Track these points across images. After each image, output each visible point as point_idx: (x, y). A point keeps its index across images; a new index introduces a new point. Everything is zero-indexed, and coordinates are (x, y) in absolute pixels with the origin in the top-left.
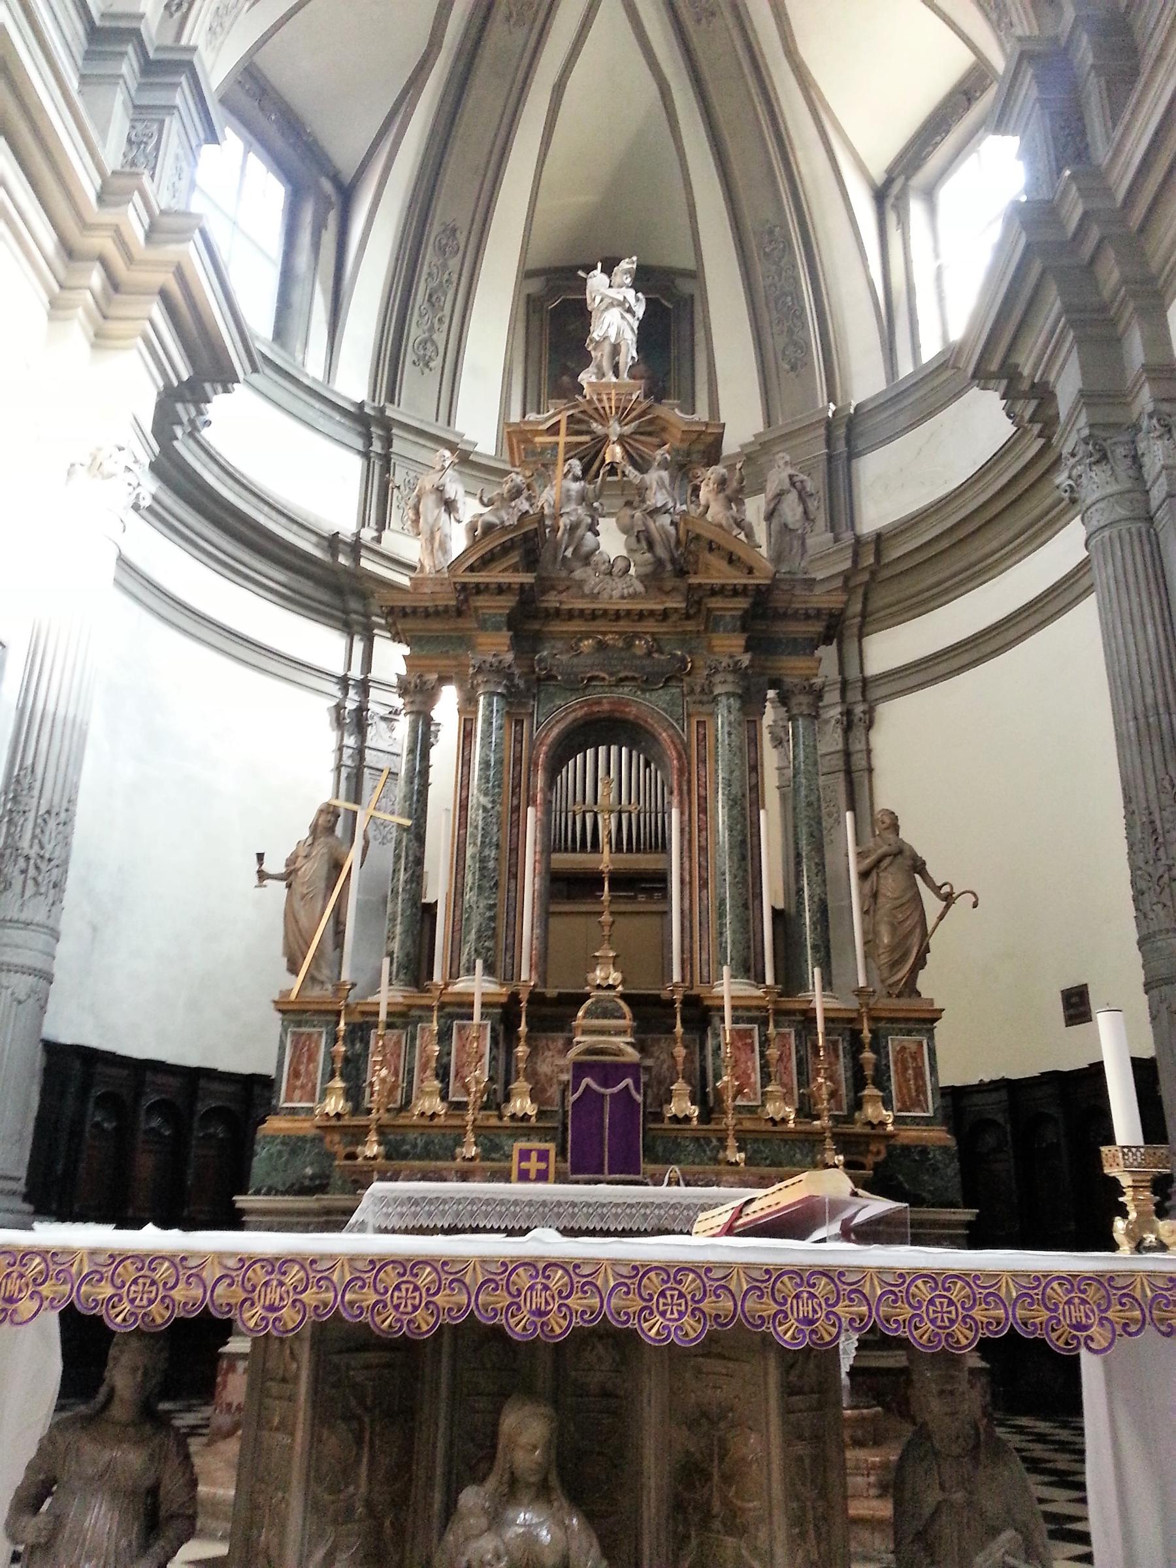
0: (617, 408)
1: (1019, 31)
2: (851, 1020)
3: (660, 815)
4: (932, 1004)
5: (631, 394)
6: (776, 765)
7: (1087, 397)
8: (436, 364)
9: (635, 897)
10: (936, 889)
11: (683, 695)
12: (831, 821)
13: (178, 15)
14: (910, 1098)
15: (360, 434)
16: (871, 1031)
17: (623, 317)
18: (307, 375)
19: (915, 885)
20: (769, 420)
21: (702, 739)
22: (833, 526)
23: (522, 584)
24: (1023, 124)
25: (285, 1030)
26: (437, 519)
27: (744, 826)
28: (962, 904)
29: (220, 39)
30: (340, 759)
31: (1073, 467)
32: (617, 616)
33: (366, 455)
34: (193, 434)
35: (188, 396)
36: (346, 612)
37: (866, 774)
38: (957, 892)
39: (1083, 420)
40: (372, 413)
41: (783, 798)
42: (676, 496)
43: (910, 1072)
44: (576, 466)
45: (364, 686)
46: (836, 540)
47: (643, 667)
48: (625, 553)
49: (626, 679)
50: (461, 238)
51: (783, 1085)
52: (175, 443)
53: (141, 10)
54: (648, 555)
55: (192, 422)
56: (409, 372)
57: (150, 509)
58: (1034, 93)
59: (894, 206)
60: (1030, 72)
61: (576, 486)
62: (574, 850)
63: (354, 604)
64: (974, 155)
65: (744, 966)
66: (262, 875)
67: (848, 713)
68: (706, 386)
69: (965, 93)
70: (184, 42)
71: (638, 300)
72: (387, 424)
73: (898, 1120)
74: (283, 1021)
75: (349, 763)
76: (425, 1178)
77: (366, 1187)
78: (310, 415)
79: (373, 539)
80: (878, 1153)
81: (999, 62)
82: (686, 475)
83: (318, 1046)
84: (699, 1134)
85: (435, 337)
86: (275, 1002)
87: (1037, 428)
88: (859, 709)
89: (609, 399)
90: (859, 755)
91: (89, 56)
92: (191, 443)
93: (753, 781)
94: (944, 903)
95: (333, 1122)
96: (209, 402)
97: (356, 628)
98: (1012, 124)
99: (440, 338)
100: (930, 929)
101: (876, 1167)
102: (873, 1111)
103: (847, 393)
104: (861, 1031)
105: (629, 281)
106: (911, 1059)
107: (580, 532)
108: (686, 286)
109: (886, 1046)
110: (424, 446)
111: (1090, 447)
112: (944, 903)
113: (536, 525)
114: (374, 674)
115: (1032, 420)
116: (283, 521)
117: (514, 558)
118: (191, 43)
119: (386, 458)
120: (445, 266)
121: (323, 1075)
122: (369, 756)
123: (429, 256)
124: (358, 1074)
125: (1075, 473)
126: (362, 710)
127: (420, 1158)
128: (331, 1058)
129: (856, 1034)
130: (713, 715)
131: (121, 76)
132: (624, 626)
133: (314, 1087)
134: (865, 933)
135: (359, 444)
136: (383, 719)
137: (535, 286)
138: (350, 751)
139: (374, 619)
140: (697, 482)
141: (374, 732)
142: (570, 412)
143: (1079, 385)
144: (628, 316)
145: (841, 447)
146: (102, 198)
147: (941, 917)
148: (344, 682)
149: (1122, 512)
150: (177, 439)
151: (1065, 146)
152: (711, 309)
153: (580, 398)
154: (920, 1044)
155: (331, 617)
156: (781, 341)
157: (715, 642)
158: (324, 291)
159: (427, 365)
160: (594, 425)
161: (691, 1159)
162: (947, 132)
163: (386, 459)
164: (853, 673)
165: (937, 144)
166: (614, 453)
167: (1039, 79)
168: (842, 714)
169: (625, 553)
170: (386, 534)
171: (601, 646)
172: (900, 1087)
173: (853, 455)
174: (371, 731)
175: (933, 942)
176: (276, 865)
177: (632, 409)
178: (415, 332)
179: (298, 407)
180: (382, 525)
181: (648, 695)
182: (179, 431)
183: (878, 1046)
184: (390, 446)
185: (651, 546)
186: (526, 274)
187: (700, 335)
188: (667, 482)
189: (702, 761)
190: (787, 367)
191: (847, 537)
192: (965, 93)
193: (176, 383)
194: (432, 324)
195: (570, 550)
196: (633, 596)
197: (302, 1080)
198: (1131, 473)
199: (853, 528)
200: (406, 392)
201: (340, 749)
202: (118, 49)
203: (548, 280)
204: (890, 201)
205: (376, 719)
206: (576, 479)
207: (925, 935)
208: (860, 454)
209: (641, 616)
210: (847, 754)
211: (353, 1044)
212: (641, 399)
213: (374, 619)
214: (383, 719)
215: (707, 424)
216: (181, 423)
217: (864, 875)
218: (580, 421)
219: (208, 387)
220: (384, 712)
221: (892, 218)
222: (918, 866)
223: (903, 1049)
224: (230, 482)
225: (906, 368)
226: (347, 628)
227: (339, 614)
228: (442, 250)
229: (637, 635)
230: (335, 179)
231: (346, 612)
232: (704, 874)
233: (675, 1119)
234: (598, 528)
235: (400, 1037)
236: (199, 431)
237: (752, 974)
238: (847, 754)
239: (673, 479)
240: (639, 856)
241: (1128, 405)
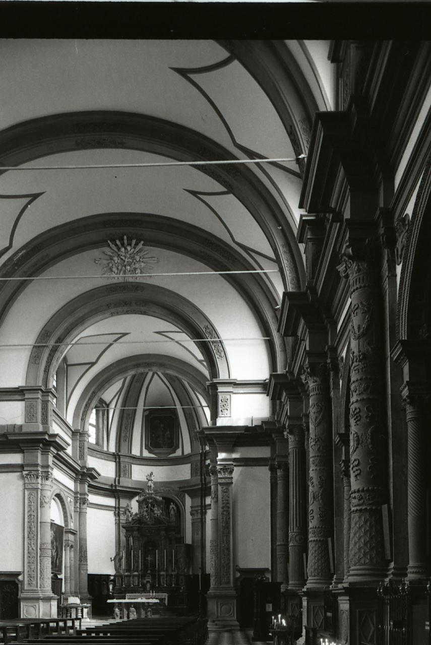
8: (127, 440)
20: (192, 451)
33: (115, 462)
36: (115, 495)
45: (119, 508)
50: (131, 416)
56: (122, 443)
63: (116, 494)
66: (111, 560)
72: (119, 456)
88: (204, 511)
91: (72, 435)
114: (121, 506)
122: (121, 521)
123: (125, 420)
126: (119, 513)
137: (147, 413)
145: (203, 458)
148: (115, 507)
163: (119, 462)
174: (121, 517)
176: (113, 559)
178: (123, 435)
201: (116, 520)
210: (202, 519)
226: (115, 497)
228: (127, 418)
230: (106, 404)
238: (202, 519)
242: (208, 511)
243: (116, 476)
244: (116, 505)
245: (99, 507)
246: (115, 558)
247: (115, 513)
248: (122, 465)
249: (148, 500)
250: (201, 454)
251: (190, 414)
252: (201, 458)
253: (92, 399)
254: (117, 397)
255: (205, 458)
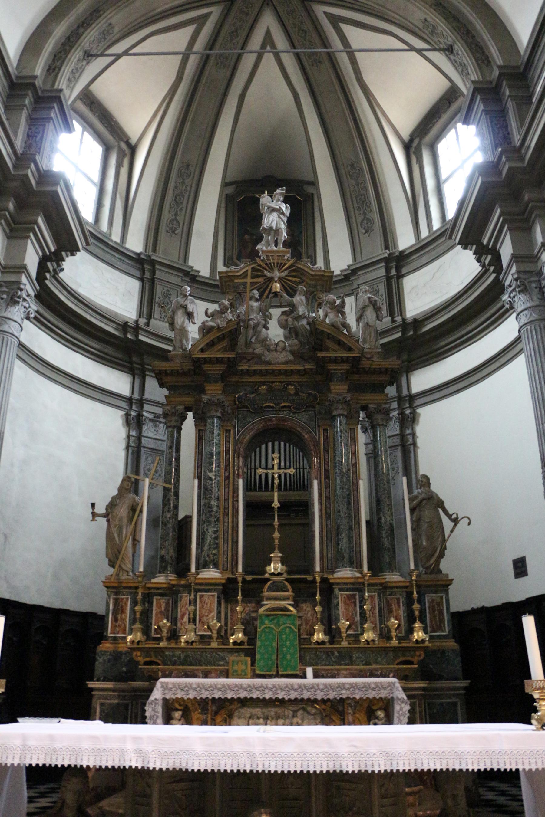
0: (278, 263)
1: (473, 78)
2: (406, 587)
3: (301, 470)
4: (448, 577)
5: (284, 256)
6: (364, 442)
7: (515, 258)
9: (289, 515)
10: (449, 516)
11: (316, 415)
12: (394, 472)
13: (53, 74)
14: (437, 625)
15: (138, 269)
16: (417, 593)
17: (279, 217)
18: (112, 241)
19: (439, 514)
21: (326, 439)
22: (391, 314)
23: (229, 358)
24: (477, 120)
25: (109, 596)
26: (183, 322)
27: (350, 486)
28: (463, 523)
29: (73, 83)
30: (128, 443)
31: (511, 292)
32: (280, 372)
33: (142, 280)
34: (55, 276)
35: (54, 258)
36: (131, 362)
37: (412, 447)
38: (460, 517)
39: (514, 269)
40: (145, 258)
41: (368, 460)
42: (309, 308)
43: (436, 612)
44: (256, 294)
46: (393, 321)
47: (293, 400)
48: (283, 339)
49: (285, 406)
50: (192, 169)
51: (372, 622)
52: (47, 282)
53: (36, 74)
54: (296, 341)
55: (54, 270)
57: (35, 318)
58: (482, 107)
59: (415, 153)
60: (479, 97)
61: (256, 304)
62: (255, 490)
64: (453, 130)
65: (350, 561)
66: (94, 515)
67: (402, 414)
68: (321, 240)
69: (447, 99)
70: (56, 87)
71: (287, 207)
72: (153, 263)
73: (431, 637)
74: (108, 592)
75: (133, 445)
76: (187, 676)
77: (157, 679)
78: (113, 260)
79: (145, 324)
80: (420, 656)
81: (464, 88)
82: (314, 297)
83: (126, 604)
84: (328, 650)
85: (178, 218)
86: (103, 582)
87: (492, 268)
88: (408, 412)
89: (273, 259)
90: (409, 437)
92: (53, 280)
93: (354, 461)
94: (453, 524)
95: (136, 646)
96: (64, 261)
97: (137, 372)
98: (471, 121)
99: (180, 218)
100: (446, 537)
101: (421, 663)
102: (418, 635)
103: (395, 245)
104: (412, 593)
105: (282, 199)
106: (437, 608)
107: (259, 328)
108: (310, 189)
109: (425, 599)
110: (172, 274)
111: (518, 283)
112: (453, 524)
113: (236, 326)
114: (147, 396)
115: (490, 264)
116: (99, 317)
117: (224, 343)
118: (60, 87)
119: (152, 281)
120: (183, 183)
121: (130, 620)
122: (144, 441)
124: (147, 619)
125: (512, 295)
126: (139, 416)
127: (182, 664)
128: (133, 612)
129: (409, 595)
130: (332, 426)
131: (25, 105)
132: (282, 378)
133: (125, 627)
134: (414, 541)
135: (138, 274)
136: (151, 420)
137: (230, 190)
138: (133, 438)
139: (146, 366)
140: (320, 301)
141: (146, 428)
142: (252, 266)
143: (512, 252)
144: (282, 216)
145: (393, 272)
146: (15, 166)
147: (452, 531)
148: (130, 400)
149: (535, 316)
150: (47, 279)
151: (498, 133)
152: (323, 200)
153: (257, 259)
154: (442, 598)
155: (122, 366)
156: (360, 218)
157: (332, 387)
158: (121, 197)
159: (173, 232)
160: (266, 272)
161: (324, 662)
162: (439, 118)
164: (405, 392)
165: (435, 123)
166: (277, 287)
167: (483, 100)
168: (399, 414)
169: (283, 339)
170: (152, 321)
171: (270, 390)
172: (431, 622)
173: (400, 276)
174: (145, 428)
175: (448, 544)
176: (101, 509)
177: (285, 264)
179: (107, 257)
180: (149, 317)
181: (296, 415)
182: (48, 275)
183: (420, 601)
184: (154, 274)
185: (297, 334)
186: (225, 184)
187: (317, 214)
188: (304, 302)
189: (326, 450)
190: (364, 231)
191: (399, 319)
192: (447, 99)
193: (48, 253)
194: (177, 212)
195: (254, 338)
196: (287, 363)
197: (119, 622)
198: (539, 296)
199: (401, 315)
200: (161, 247)
201: (129, 437)
202: (24, 93)
203: (237, 187)
204: (412, 150)
205: (147, 421)
206: (257, 300)
207: (444, 541)
208: (403, 276)
209: (292, 372)
210: (402, 436)
211: (144, 604)
212: (290, 258)
213: (146, 366)
214: (151, 420)
215: (324, 271)
216: (49, 271)
217: (412, 510)
218: (258, 270)
219: (64, 254)
220: (150, 416)
221: (414, 159)
222: (440, 504)
223: (433, 601)
224: (73, 299)
225: (424, 233)
227: (128, 365)
229: (290, 383)
230: (128, 143)
231: (131, 362)
232: (328, 510)
233: (317, 643)
234: (268, 326)
235: (169, 600)
236: (58, 274)
237: (355, 565)
239: (307, 299)
240: (291, 492)
241: (537, 262)
242: (419, 411)
243: (140, 315)
244: (133, 393)
245: (72, 385)
246: (112, 505)
247: (127, 415)
248: (159, 290)
249: (268, 274)
250: (387, 261)
251: (352, 165)
252: (388, 270)
253: (89, 25)
254: (164, 105)
255: (398, 269)
